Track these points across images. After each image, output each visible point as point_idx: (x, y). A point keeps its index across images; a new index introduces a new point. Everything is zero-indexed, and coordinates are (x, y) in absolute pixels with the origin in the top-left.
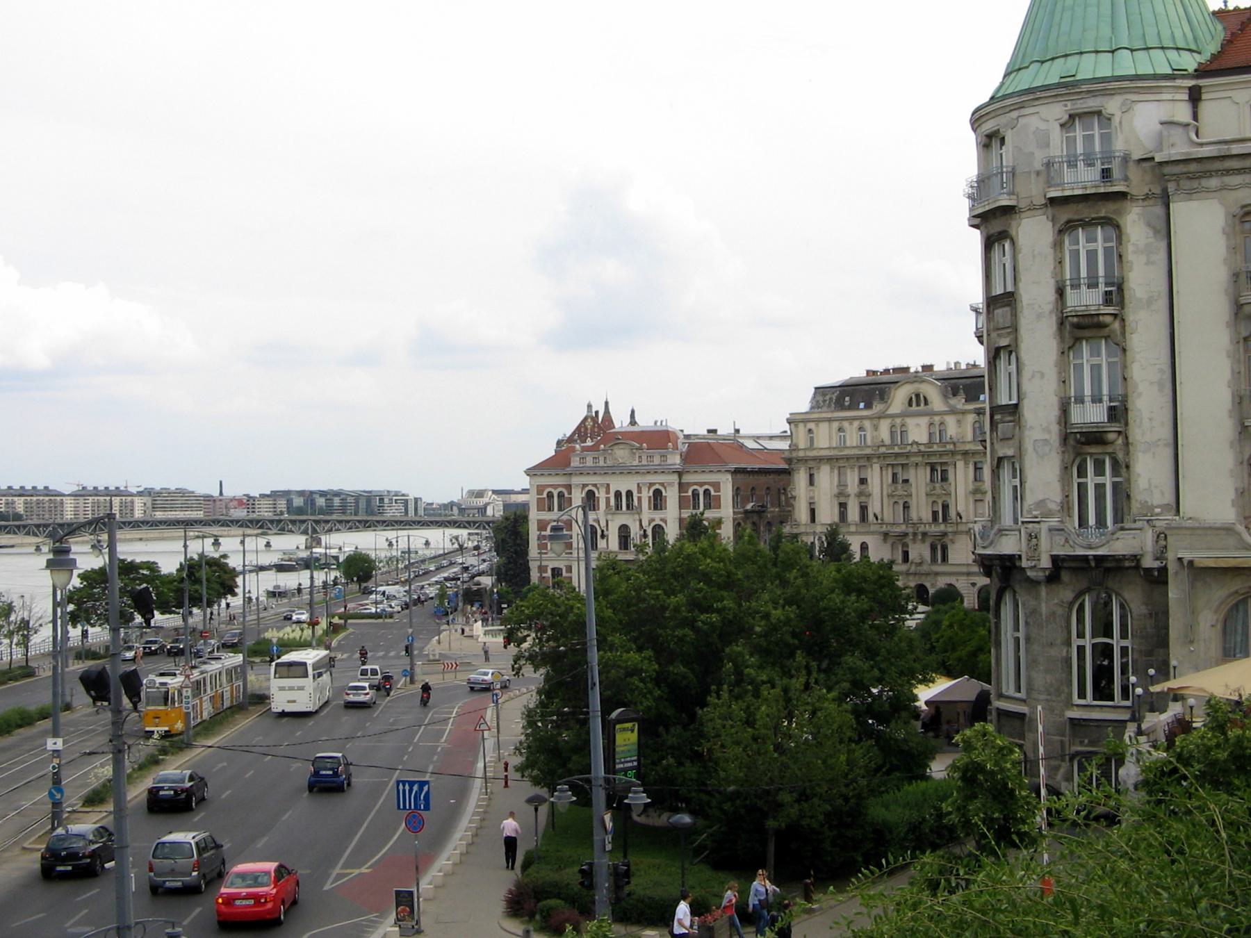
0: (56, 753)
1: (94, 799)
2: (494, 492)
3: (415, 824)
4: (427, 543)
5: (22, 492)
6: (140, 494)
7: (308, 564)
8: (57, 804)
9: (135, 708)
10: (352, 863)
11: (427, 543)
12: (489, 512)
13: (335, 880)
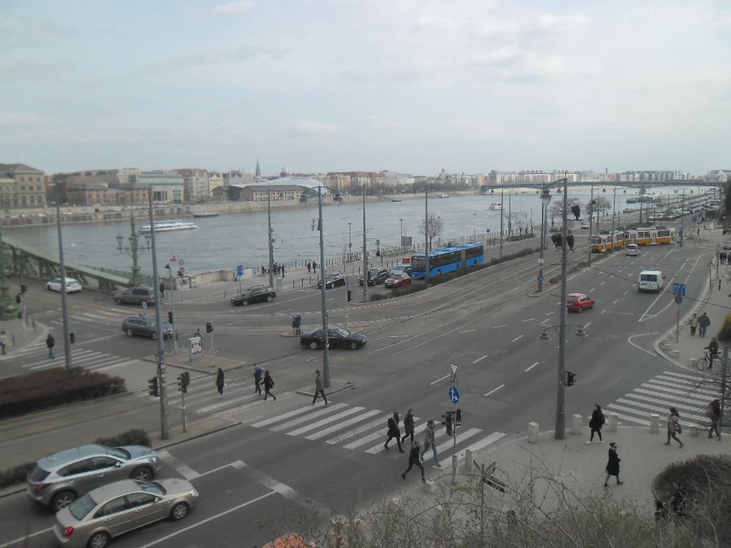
0: (541, 264)
1: (552, 282)
2: (723, 171)
3: (678, 300)
4: (692, 192)
5: (532, 173)
6: (575, 173)
7: (641, 200)
8: (540, 282)
9: (571, 249)
10: (651, 312)
11: (692, 192)
12: (720, 180)
13: (644, 318)
